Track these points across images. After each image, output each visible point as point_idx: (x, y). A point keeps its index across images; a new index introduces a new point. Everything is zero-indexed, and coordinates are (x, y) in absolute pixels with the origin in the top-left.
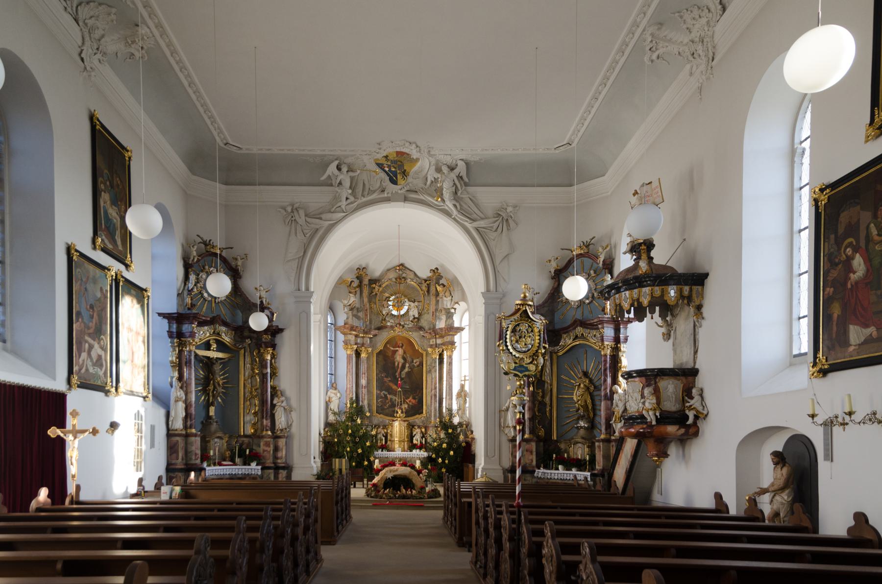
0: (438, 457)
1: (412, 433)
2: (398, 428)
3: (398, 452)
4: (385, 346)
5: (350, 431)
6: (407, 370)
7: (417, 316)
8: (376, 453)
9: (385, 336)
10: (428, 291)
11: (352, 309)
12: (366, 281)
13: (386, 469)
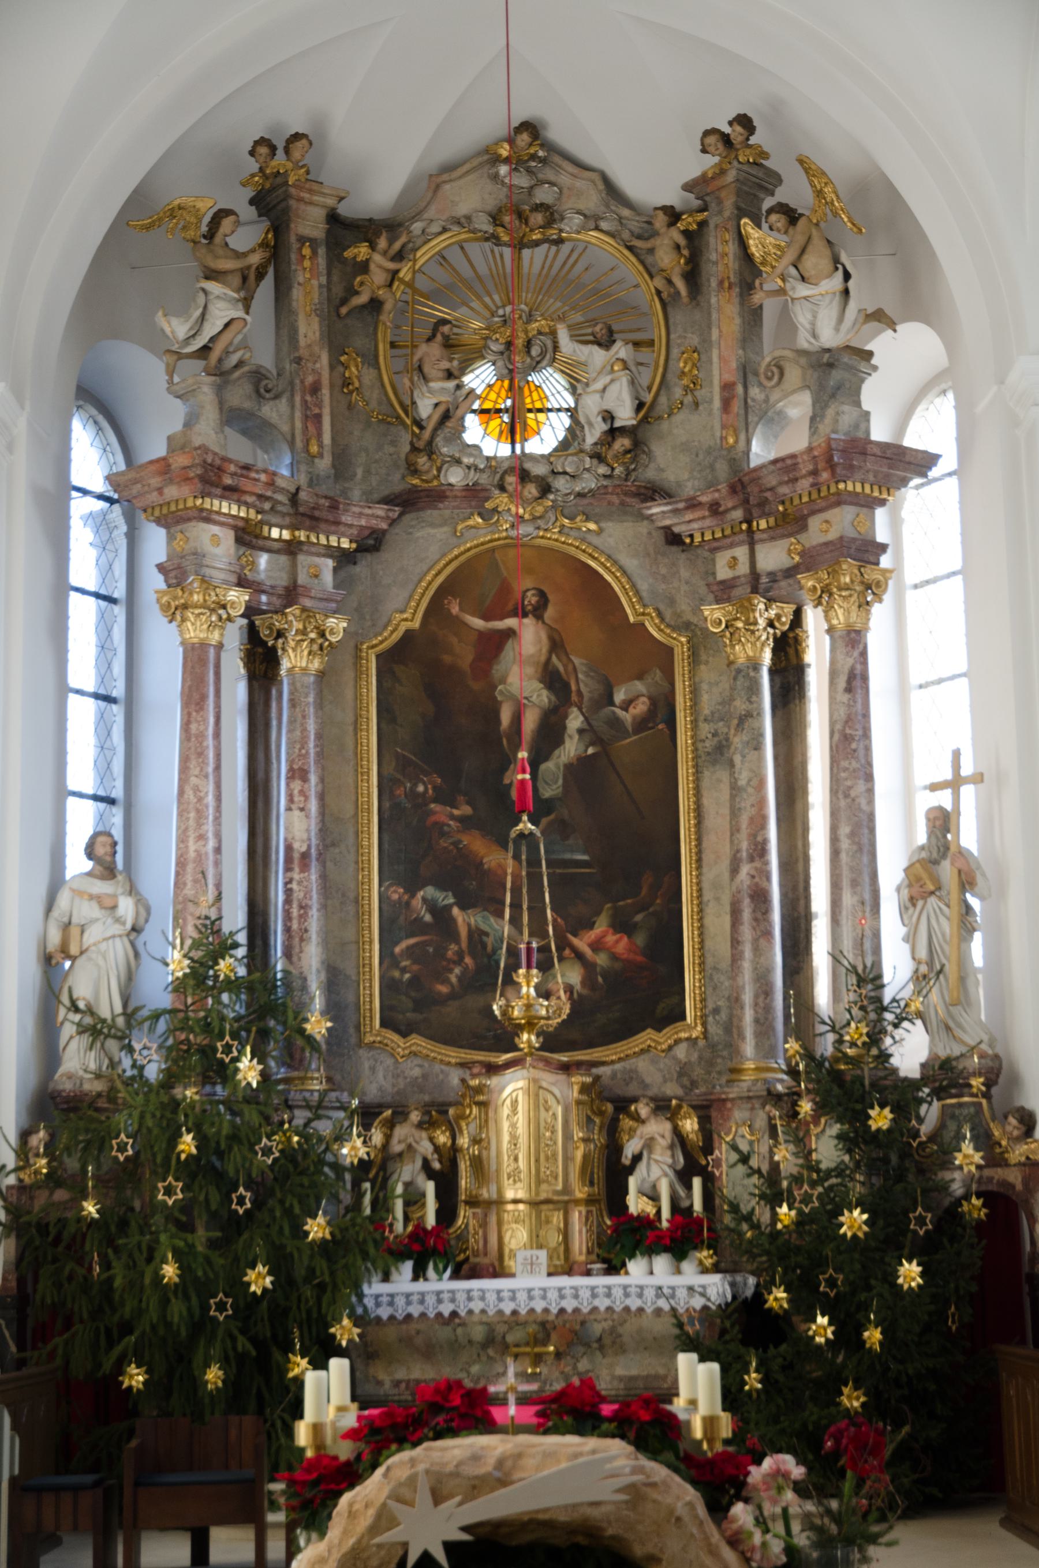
0: (806, 1303)
1: (614, 1148)
2: (523, 1113)
3: (529, 1282)
4: (436, 609)
5: (187, 1144)
6: (571, 748)
7: (625, 416)
8: (374, 1288)
9: (431, 548)
10: (693, 276)
11: (221, 374)
12: (310, 222)
13: (402, 1463)
